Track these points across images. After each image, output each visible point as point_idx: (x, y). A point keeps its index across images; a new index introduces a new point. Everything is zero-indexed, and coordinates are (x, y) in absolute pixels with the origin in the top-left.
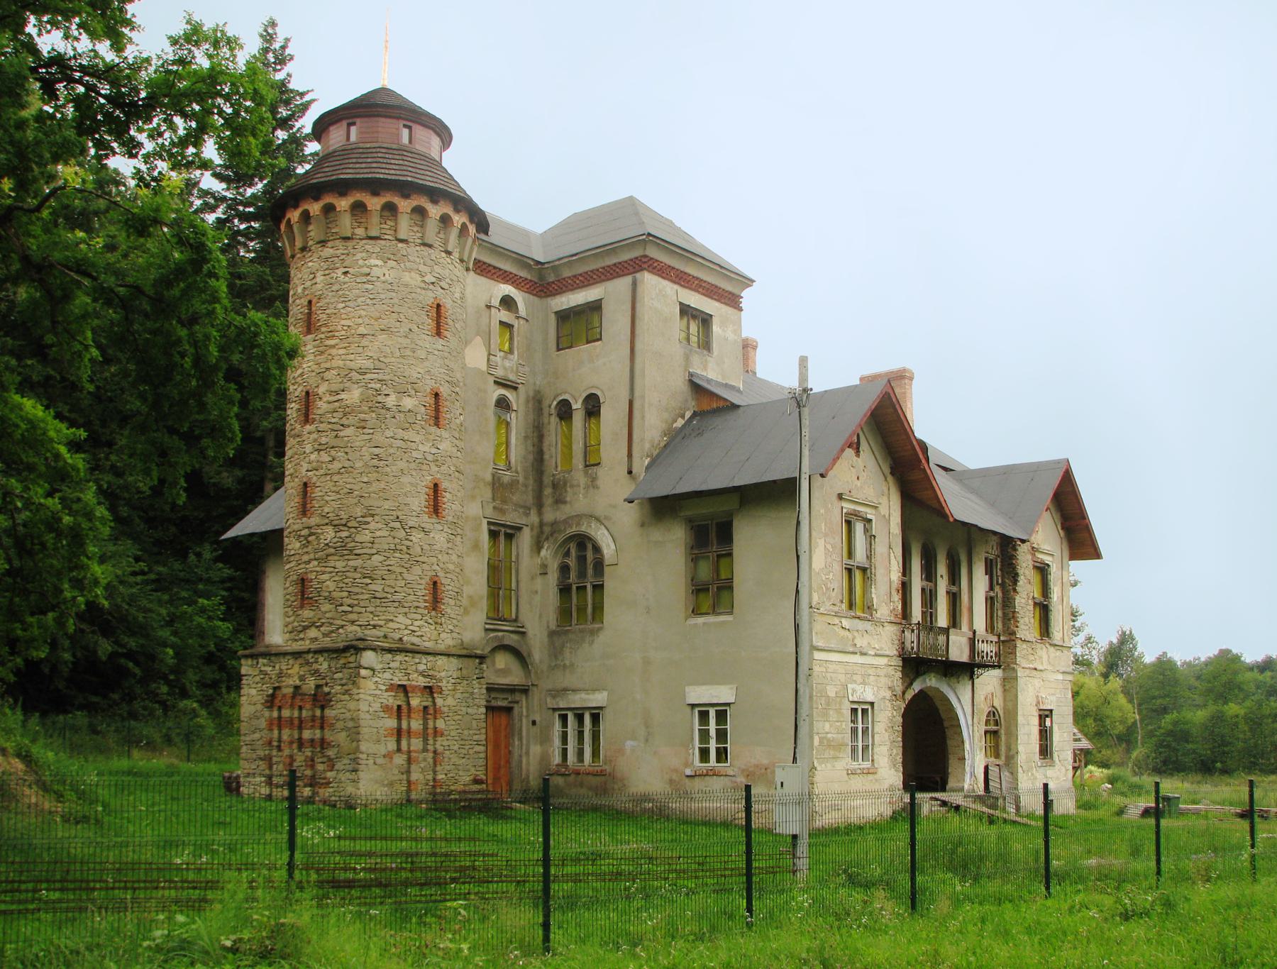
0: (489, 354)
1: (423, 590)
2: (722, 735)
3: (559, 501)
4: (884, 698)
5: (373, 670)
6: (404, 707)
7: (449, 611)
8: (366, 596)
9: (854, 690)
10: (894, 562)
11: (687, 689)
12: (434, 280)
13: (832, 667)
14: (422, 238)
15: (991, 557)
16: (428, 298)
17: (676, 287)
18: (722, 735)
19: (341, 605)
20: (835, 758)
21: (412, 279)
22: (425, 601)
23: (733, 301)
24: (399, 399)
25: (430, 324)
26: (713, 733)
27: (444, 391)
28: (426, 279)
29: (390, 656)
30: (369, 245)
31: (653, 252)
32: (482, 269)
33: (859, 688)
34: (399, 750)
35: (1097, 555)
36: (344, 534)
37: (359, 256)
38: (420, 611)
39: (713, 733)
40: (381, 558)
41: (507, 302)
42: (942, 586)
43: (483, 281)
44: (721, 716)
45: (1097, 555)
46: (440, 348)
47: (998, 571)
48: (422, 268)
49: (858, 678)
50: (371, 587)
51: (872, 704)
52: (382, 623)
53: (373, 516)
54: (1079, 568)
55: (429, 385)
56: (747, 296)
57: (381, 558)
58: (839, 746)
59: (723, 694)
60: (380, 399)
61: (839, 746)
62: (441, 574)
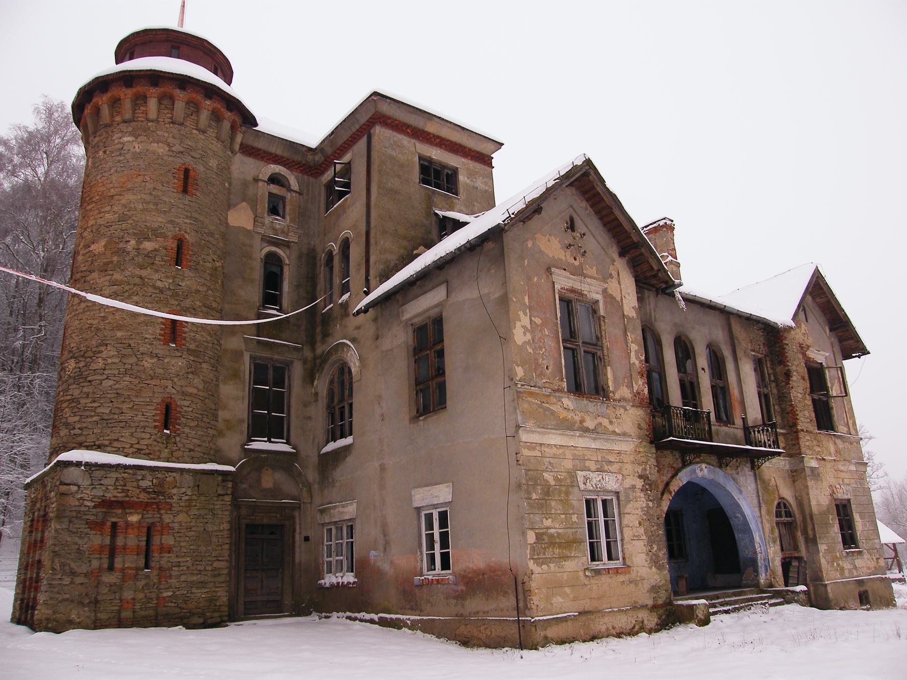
0: (256, 216)
1: (153, 413)
2: (444, 537)
3: (326, 335)
4: (633, 487)
5: (79, 487)
6: (121, 523)
7: (187, 430)
8: (95, 418)
9: (586, 479)
10: (634, 347)
11: (413, 493)
12: (182, 149)
13: (549, 452)
14: (171, 118)
15: (760, 356)
16: (178, 162)
17: (413, 141)
18: (444, 537)
19: (74, 428)
20: (566, 558)
21: (161, 149)
22: (155, 421)
23: (486, 160)
24: (139, 242)
25: (177, 183)
26: (437, 537)
27: (190, 238)
28: (174, 149)
29: (103, 472)
30: (123, 127)
31: (385, 108)
32: (249, 151)
33: (595, 477)
34: (111, 568)
35: (864, 352)
36: (82, 364)
37: (116, 136)
38: (148, 430)
40: (111, 383)
41: (274, 179)
42: (721, 402)
43: (251, 162)
44: (443, 516)
45: (864, 352)
46: (187, 203)
47: (767, 369)
48: (171, 140)
49: (593, 466)
50: (99, 410)
51: (617, 494)
52: (107, 443)
53: (107, 345)
54: (850, 365)
55: (171, 231)
56: (498, 158)
57: (111, 383)
58: (572, 543)
59: (442, 494)
60: (122, 245)
61: (572, 543)
62: (177, 397)
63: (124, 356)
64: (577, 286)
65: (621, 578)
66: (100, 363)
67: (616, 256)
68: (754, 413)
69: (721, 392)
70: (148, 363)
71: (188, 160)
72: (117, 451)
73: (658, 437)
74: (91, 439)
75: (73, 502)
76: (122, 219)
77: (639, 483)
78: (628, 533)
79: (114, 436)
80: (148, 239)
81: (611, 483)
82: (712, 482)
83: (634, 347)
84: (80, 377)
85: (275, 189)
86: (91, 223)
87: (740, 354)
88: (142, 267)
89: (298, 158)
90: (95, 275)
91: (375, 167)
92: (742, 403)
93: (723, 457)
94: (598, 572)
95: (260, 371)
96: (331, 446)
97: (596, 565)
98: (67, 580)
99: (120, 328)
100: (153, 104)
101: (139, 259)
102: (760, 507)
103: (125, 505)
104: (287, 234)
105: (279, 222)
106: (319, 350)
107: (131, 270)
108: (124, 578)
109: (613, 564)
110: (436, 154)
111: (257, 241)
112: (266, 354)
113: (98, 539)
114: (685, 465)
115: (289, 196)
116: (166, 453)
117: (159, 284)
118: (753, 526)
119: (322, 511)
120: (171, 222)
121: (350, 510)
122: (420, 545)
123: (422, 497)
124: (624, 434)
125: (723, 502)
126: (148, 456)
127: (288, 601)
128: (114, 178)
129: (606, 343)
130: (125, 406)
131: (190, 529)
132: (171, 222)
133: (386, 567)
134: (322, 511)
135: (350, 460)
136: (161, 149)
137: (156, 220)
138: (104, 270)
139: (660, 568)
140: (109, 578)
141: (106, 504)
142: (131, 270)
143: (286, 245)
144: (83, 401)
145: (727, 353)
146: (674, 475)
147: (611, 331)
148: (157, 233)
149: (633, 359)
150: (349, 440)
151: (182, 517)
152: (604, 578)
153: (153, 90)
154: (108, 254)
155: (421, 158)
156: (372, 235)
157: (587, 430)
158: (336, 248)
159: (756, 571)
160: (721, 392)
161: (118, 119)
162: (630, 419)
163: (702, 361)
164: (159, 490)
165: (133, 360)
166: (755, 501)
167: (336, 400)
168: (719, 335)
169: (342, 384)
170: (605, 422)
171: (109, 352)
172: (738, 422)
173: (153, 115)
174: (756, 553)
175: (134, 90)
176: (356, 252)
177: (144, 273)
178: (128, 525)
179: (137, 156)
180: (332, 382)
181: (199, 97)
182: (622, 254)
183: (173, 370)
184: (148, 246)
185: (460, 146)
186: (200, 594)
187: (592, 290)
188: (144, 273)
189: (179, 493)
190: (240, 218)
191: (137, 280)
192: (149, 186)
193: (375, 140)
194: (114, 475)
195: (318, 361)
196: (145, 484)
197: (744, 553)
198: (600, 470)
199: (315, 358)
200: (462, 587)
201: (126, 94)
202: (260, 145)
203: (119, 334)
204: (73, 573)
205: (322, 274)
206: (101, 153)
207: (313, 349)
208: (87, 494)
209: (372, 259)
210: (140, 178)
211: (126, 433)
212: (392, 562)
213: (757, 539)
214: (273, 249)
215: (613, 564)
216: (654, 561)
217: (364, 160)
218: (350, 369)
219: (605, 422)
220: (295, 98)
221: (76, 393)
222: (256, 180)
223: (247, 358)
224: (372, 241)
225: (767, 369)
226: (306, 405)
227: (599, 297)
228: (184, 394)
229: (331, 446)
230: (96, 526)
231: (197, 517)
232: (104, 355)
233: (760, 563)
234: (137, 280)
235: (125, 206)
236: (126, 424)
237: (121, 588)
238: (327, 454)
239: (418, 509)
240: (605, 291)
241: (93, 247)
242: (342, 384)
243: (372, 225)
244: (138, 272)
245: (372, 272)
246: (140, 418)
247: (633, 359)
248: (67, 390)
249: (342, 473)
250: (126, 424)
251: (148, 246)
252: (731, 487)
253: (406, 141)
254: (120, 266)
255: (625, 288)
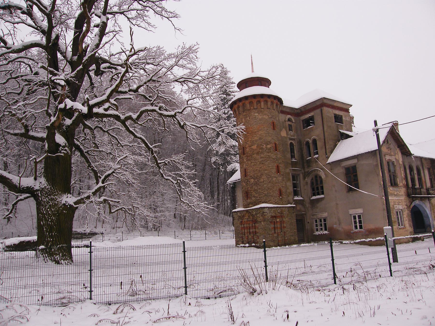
1: (277, 192)
3: (309, 166)
10: (402, 172)
16: (271, 120)
18: (360, 222)
21: (266, 117)
23: (347, 111)
24: (266, 146)
25: (272, 127)
26: (357, 218)
27: (277, 143)
30: (254, 110)
31: (325, 101)
32: (283, 112)
34: (275, 233)
37: (252, 113)
39: (357, 218)
41: (289, 120)
44: (359, 217)
47: (431, 171)
51: (402, 210)
56: (351, 109)
59: (360, 211)
63: (268, 178)
64: (390, 158)
65: (404, 230)
66: (262, 180)
67: (397, 148)
68: (429, 185)
69: (420, 179)
70: (274, 179)
71: (273, 119)
72: (271, 203)
73: (408, 195)
74: (263, 200)
75: (266, 217)
76: (260, 139)
77: (406, 207)
78: (405, 219)
79: (269, 199)
80: (268, 144)
81: (401, 207)
82: (419, 205)
83: (402, 172)
84: (256, 184)
85: (289, 123)
86: (250, 139)
87: (424, 167)
88: (268, 153)
89: (293, 112)
90: (255, 155)
91: (325, 120)
92: (425, 182)
93: (422, 199)
94: (400, 228)
95: (293, 177)
96: (314, 198)
97: (400, 227)
98: (268, 236)
99: (266, 170)
100: (262, 104)
101: (267, 151)
102: (431, 210)
103: (276, 217)
104: (294, 136)
105: (292, 133)
106: (307, 170)
107: (266, 154)
108: (278, 235)
109: (402, 227)
110: (338, 112)
111: (288, 140)
112: (294, 173)
113: (272, 226)
114: (413, 201)
115: (292, 124)
116: (281, 203)
117: (273, 157)
118: (429, 216)
119: (313, 215)
120: (273, 139)
121: (325, 215)
122: (352, 223)
123: (352, 212)
124: (402, 195)
125: (421, 209)
126: (278, 204)
127: (306, 239)
128: (255, 126)
129: (397, 172)
130: (271, 191)
131: (288, 222)
132: (273, 139)
133: (340, 229)
134: (313, 215)
135: (323, 202)
136: (266, 117)
137: (269, 139)
138: (258, 153)
139: (411, 227)
140: (275, 235)
141: (272, 217)
142: (266, 154)
143: (294, 139)
144: (259, 190)
145: (421, 168)
146: (411, 204)
147: (397, 168)
148: (270, 143)
149: (403, 176)
150: (322, 196)
151: (287, 219)
152: (401, 230)
153: (262, 99)
154: (258, 149)
155: (334, 114)
156: (326, 140)
157: (395, 195)
158: (310, 141)
159: (430, 228)
160: (420, 179)
161: (252, 108)
162: (402, 191)
163: (415, 172)
164: (282, 213)
165: (271, 179)
166: (430, 209)
167: (315, 184)
168: (419, 163)
169: (317, 180)
170: (398, 192)
171: (264, 177)
172: (424, 187)
173: (262, 107)
174: (430, 223)
175: (257, 100)
176: (319, 144)
177: (269, 154)
178: (277, 222)
179: (260, 120)
180: (312, 179)
181: (273, 100)
182: (398, 147)
183: (280, 181)
184: (269, 146)
185: (342, 108)
186: (292, 238)
187: (393, 159)
188: (269, 154)
189: (286, 212)
190: (284, 133)
191: (268, 156)
192: (266, 129)
193: (323, 112)
194: (273, 209)
195: (306, 173)
196: (279, 211)
197: (426, 223)
198: (398, 204)
199: (305, 172)
200: (367, 233)
201: (255, 101)
202: (284, 109)
203: (266, 172)
204: (269, 234)
205: (305, 148)
206: (248, 118)
207: (304, 170)
208: (269, 215)
209: (327, 147)
210: (263, 127)
211: (272, 198)
212: (342, 228)
213: (431, 219)
214: (291, 141)
215: (402, 227)
216: (410, 226)
217: (320, 116)
218: (320, 177)
219: (398, 192)
220: (295, 97)
221: (256, 188)
222: (285, 121)
223: (291, 175)
224: (326, 142)
225: (431, 171)
226: (304, 186)
227: (394, 160)
228: (283, 187)
229: (314, 198)
230: (271, 222)
231: (290, 219)
232: (263, 178)
233: (432, 226)
234: (268, 156)
235: (260, 135)
236: (272, 196)
237: (278, 237)
238: (313, 200)
239: (351, 215)
240: (395, 159)
241: (252, 147)
242: (317, 180)
243: (326, 137)
244: (267, 154)
245: (327, 151)
246: (274, 194)
247: (403, 176)
248: (252, 187)
249: (320, 205)
250: (272, 196)
251: (269, 146)
252: (424, 206)
253: (330, 110)
254: (262, 153)
255: (399, 157)
